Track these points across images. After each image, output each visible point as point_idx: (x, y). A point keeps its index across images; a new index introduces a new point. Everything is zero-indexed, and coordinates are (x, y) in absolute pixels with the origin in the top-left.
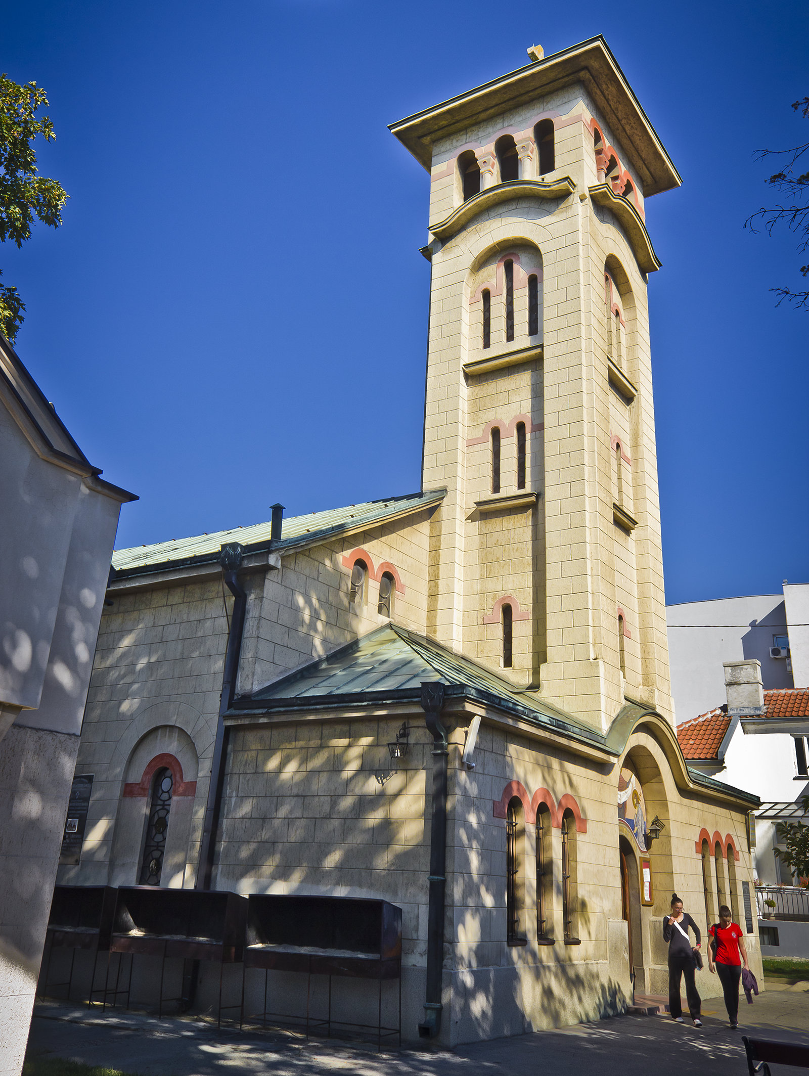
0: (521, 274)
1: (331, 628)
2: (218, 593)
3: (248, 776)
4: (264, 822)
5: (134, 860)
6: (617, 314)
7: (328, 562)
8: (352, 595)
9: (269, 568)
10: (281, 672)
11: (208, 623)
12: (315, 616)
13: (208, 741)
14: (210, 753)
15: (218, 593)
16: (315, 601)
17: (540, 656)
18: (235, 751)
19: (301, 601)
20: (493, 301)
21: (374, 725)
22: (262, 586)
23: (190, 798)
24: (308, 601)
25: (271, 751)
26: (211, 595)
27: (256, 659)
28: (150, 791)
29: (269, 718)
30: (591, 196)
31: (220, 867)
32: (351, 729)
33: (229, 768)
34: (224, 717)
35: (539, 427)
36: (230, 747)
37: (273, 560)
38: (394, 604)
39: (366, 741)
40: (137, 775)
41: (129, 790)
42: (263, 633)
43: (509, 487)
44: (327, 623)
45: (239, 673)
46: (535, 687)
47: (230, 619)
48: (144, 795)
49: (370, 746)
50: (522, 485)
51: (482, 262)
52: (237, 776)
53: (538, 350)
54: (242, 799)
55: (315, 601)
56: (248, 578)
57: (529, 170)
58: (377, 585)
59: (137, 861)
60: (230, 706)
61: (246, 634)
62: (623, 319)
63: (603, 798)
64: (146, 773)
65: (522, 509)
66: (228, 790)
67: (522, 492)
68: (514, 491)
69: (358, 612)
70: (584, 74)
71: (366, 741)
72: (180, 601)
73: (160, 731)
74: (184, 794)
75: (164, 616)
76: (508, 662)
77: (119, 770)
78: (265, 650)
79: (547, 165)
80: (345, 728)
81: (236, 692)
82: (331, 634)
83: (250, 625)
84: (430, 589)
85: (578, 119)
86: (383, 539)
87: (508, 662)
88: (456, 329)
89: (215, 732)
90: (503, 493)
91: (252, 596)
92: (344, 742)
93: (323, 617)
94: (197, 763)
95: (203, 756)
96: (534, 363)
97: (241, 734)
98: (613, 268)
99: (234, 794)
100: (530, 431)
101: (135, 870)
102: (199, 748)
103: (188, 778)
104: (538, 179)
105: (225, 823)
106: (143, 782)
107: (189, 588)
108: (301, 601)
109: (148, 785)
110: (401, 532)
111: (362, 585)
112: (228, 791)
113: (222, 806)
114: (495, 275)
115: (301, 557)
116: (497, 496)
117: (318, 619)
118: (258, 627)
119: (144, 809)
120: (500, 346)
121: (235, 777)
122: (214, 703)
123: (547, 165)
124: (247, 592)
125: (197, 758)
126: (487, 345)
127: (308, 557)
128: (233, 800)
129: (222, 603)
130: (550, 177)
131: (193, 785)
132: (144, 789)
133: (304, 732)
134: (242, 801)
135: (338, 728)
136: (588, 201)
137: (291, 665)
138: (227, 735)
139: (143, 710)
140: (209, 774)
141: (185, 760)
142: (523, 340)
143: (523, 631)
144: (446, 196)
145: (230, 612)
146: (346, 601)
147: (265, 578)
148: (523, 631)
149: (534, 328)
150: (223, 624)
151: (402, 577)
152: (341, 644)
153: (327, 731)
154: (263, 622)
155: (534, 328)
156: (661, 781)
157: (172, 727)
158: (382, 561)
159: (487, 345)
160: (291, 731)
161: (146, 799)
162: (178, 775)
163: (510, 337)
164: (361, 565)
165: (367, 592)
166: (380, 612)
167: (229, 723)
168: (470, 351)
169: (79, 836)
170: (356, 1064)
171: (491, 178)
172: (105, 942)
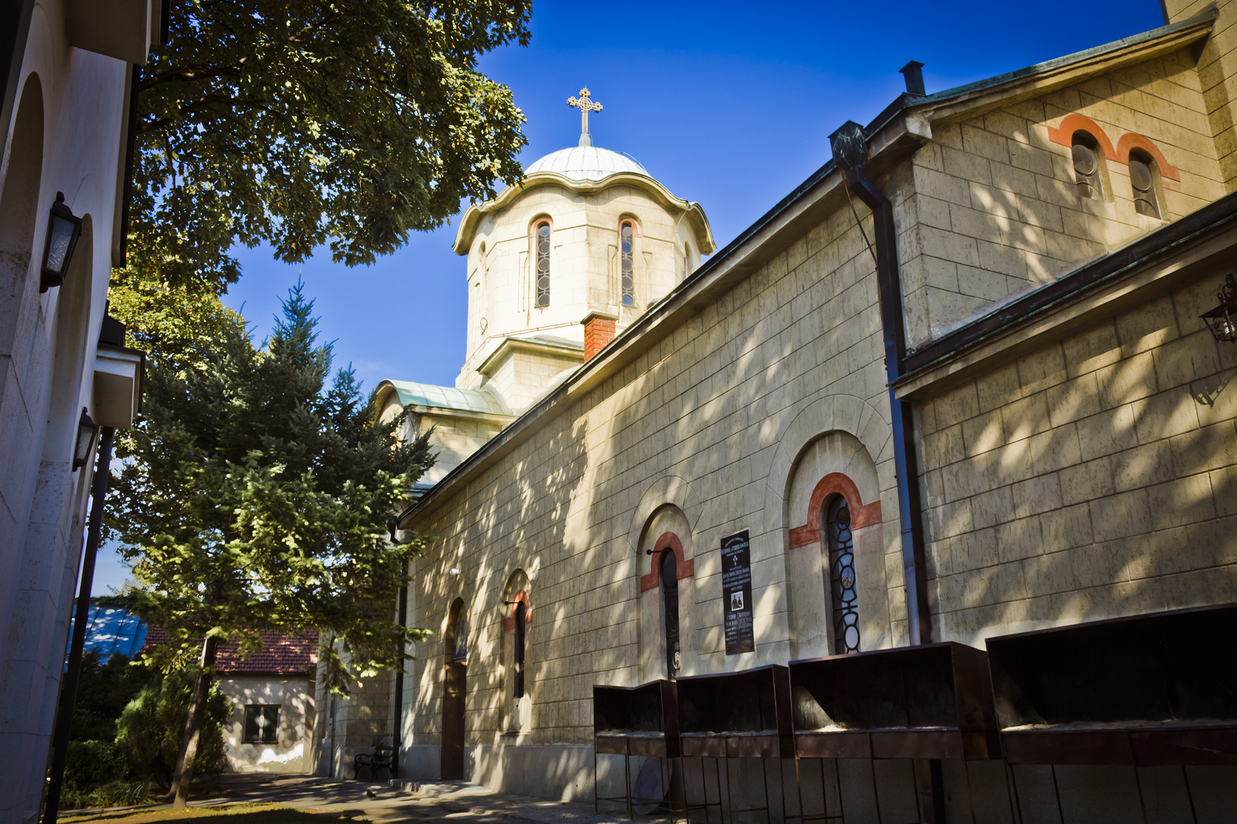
1: (1054, 238)
2: (850, 221)
3: (955, 467)
4: (997, 531)
5: (821, 630)
7: (1020, 138)
8: (1082, 189)
9: (913, 145)
10: (978, 308)
11: (847, 269)
12: (1018, 220)
13: (882, 438)
14: (890, 451)
15: (850, 221)
16: (1010, 196)
18: (925, 437)
19: (985, 198)
21: (1165, 305)
22: (910, 179)
23: (877, 526)
24: (998, 197)
25: (981, 418)
26: (841, 230)
27: (927, 287)
28: (823, 533)
29: (965, 361)
31: (942, 617)
32: (1115, 327)
33: (922, 466)
34: (893, 386)
36: (917, 434)
37: (915, 125)
38: (1163, 200)
39: (1152, 340)
40: (801, 516)
41: (795, 539)
42: (928, 248)
44: (1046, 230)
45: (906, 319)
47: (874, 249)
48: (816, 540)
49: (1164, 345)
52: (937, 473)
54: (953, 505)
55: (1010, 196)
56: (888, 177)
59: (825, 633)
60: (901, 372)
61: (902, 258)
64: (811, 509)
66: (930, 498)
69: (1096, 211)
71: (1152, 340)
72: (804, 258)
73: (817, 446)
74: (867, 524)
75: (788, 287)
77: (776, 516)
78: (940, 274)
80: (1107, 332)
81: (908, 347)
82: (1057, 246)
83: (905, 246)
84: (1224, 170)
86: (1116, 98)
89: (888, 418)
91: (900, 199)
92: (1112, 355)
93: (1033, 220)
94: (876, 473)
95: (881, 460)
97: (929, 408)
99: (940, 501)
101: (825, 644)
102: (872, 446)
103: (868, 498)
105: (936, 552)
106: (810, 523)
107: (811, 235)
108: (985, 198)
109: (818, 525)
110: (1148, 88)
111: (1096, 173)
112: (929, 499)
113: (924, 524)
115: (970, 132)
117: (1026, 223)
118: (919, 239)
119: (819, 561)
121: (935, 476)
122: (880, 374)
124: (891, 198)
125: (872, 464)
127: (985, 129)
128: (940, 510)
129: (859, 232)
131: (876, 506)
132: (813, 532)
133: (1032, 366)
134: (954, 510)
135: (1093, 337)
137: (994, 296)
138: (907, 413)
139: (789, 425)
140: (894, 482)
141: (858, 475)
145: (872, 240)
146: (1070, 197)
147: (912, 165)
150: (868, 260)
151: (1167, 154)
152: (1077, 261)
153: (1072, 350)
154: (924, 231)
157: (830, 434)
158: (1123, 132)
160: (1009, 374)
161: (819, 544)
162: (854, 499)
164: (1086, 141)
165: (1108, 182)
166: (1139, 209)
167: (903, 392)
169: (747, 613)
170: (225, 808)
172: (788, 747)
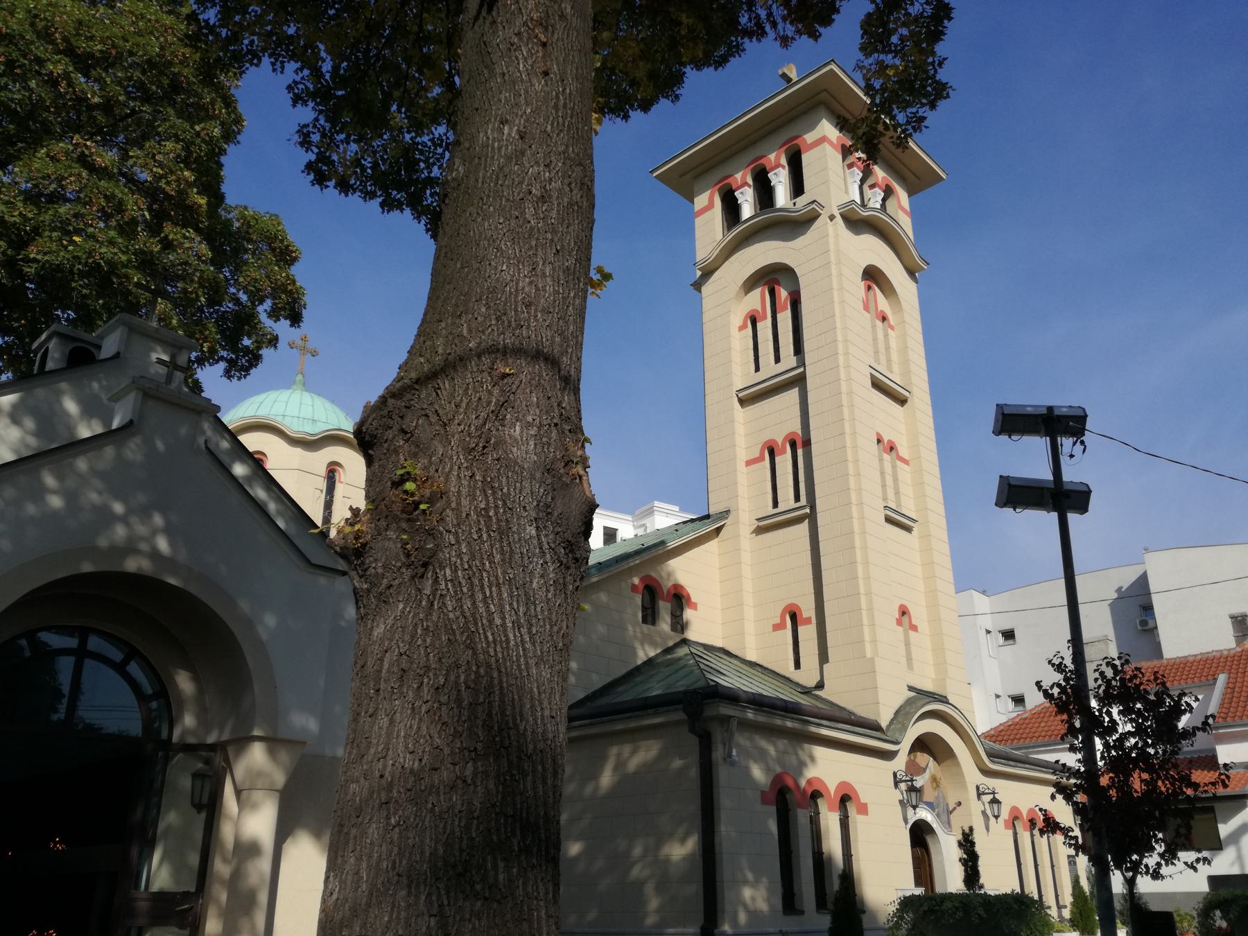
0: (783, 294)
6: (884, 319)
7: (587, 607)
17: (824, 657)
20: (759, 325)
30: (841, 215)
35: (807, 443)
43: (787, 498)
46: (820, 686)
50: (797, 498)
51: (751, 283)
53: (802, 370)
57: (782, 196)
58: (669, 605)
62: (892, 323)
63: (871, 779)
65: (798, 520)
67: (798, 505)
68: (792, 504)
70: (824, 96)
76: (797, 665)
79: (798, 188)
85: (823, 139)
87: (797, 665)
88: (730, 356)
90: (781, 508)
96: (799, 381)
98: (872, 275)
100: (801, 443)
104: (790, 205)
114: (756, 299)
116: (776, 511)
120: (769, 368)
123: (798, 188)
126: (757, 369)
130: (802, 201)
136: (839, 219)
142: (788, 359)
143: (808, 633)
144: (709, 228)
148: (808, 633)
149: (798, 349)
155: (798, 349)
156: (958, 764)
159: (757, 369)
163: (777, 360)
168: (742, 375)
171: (747, 211)
